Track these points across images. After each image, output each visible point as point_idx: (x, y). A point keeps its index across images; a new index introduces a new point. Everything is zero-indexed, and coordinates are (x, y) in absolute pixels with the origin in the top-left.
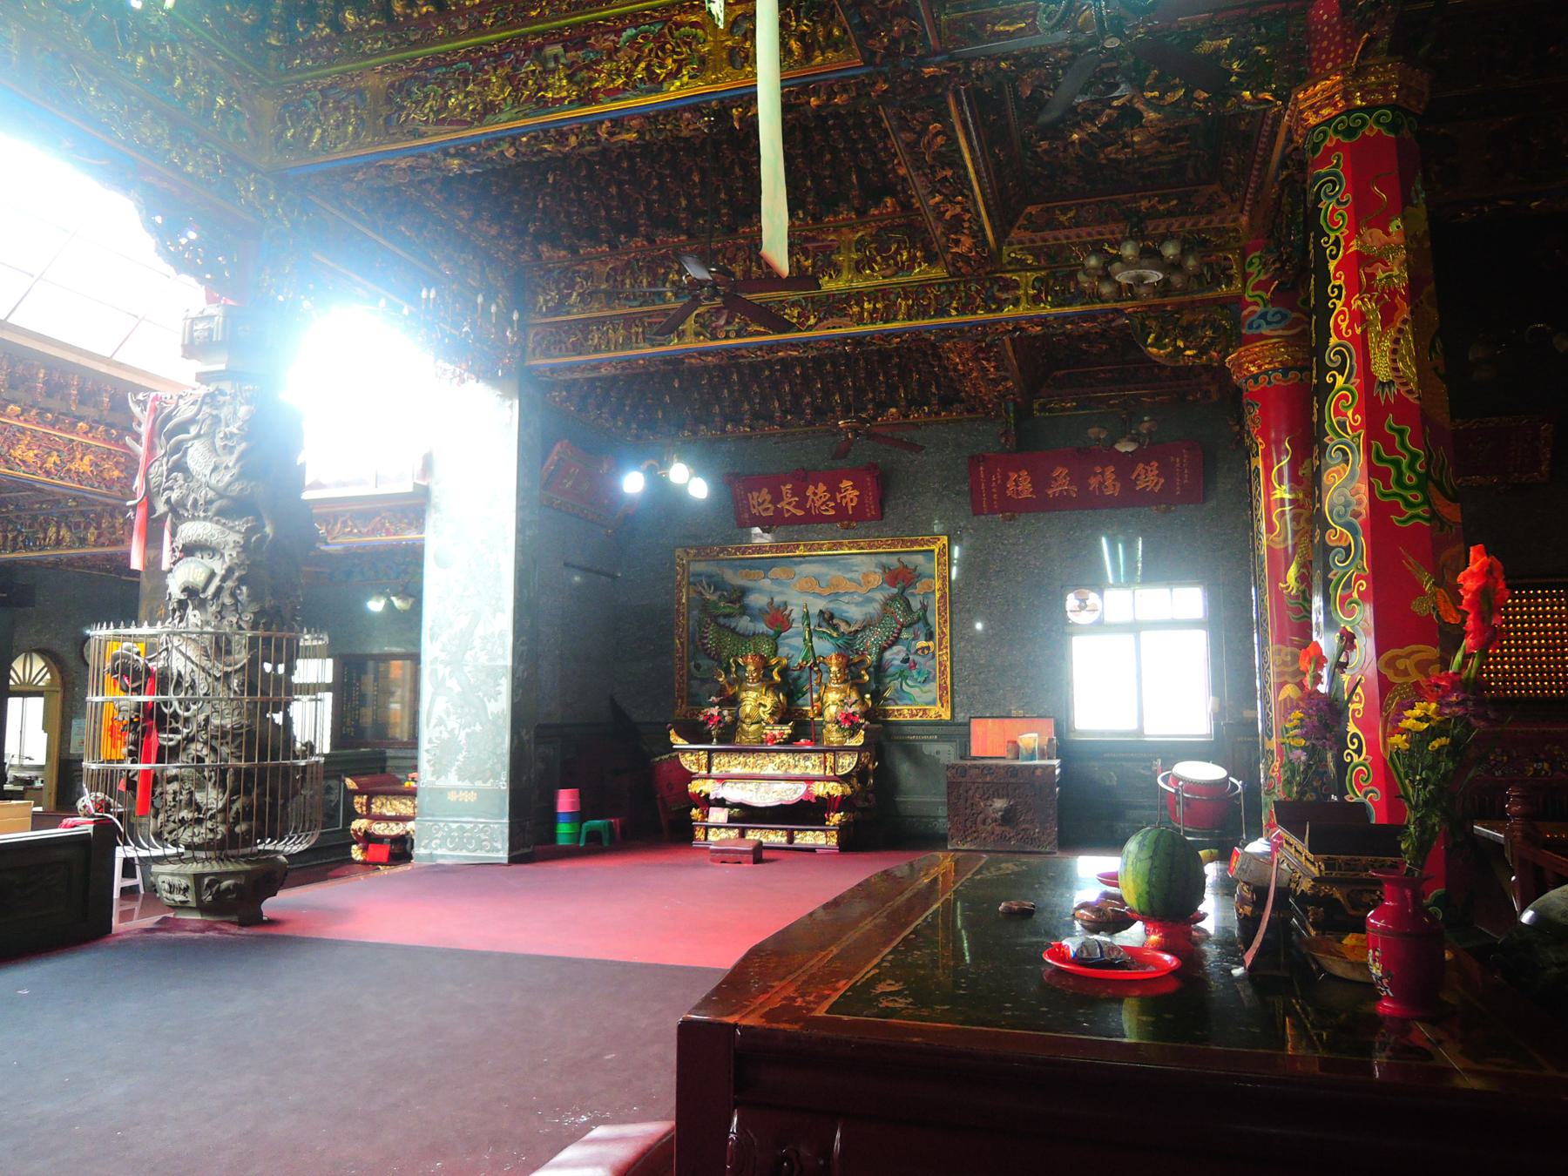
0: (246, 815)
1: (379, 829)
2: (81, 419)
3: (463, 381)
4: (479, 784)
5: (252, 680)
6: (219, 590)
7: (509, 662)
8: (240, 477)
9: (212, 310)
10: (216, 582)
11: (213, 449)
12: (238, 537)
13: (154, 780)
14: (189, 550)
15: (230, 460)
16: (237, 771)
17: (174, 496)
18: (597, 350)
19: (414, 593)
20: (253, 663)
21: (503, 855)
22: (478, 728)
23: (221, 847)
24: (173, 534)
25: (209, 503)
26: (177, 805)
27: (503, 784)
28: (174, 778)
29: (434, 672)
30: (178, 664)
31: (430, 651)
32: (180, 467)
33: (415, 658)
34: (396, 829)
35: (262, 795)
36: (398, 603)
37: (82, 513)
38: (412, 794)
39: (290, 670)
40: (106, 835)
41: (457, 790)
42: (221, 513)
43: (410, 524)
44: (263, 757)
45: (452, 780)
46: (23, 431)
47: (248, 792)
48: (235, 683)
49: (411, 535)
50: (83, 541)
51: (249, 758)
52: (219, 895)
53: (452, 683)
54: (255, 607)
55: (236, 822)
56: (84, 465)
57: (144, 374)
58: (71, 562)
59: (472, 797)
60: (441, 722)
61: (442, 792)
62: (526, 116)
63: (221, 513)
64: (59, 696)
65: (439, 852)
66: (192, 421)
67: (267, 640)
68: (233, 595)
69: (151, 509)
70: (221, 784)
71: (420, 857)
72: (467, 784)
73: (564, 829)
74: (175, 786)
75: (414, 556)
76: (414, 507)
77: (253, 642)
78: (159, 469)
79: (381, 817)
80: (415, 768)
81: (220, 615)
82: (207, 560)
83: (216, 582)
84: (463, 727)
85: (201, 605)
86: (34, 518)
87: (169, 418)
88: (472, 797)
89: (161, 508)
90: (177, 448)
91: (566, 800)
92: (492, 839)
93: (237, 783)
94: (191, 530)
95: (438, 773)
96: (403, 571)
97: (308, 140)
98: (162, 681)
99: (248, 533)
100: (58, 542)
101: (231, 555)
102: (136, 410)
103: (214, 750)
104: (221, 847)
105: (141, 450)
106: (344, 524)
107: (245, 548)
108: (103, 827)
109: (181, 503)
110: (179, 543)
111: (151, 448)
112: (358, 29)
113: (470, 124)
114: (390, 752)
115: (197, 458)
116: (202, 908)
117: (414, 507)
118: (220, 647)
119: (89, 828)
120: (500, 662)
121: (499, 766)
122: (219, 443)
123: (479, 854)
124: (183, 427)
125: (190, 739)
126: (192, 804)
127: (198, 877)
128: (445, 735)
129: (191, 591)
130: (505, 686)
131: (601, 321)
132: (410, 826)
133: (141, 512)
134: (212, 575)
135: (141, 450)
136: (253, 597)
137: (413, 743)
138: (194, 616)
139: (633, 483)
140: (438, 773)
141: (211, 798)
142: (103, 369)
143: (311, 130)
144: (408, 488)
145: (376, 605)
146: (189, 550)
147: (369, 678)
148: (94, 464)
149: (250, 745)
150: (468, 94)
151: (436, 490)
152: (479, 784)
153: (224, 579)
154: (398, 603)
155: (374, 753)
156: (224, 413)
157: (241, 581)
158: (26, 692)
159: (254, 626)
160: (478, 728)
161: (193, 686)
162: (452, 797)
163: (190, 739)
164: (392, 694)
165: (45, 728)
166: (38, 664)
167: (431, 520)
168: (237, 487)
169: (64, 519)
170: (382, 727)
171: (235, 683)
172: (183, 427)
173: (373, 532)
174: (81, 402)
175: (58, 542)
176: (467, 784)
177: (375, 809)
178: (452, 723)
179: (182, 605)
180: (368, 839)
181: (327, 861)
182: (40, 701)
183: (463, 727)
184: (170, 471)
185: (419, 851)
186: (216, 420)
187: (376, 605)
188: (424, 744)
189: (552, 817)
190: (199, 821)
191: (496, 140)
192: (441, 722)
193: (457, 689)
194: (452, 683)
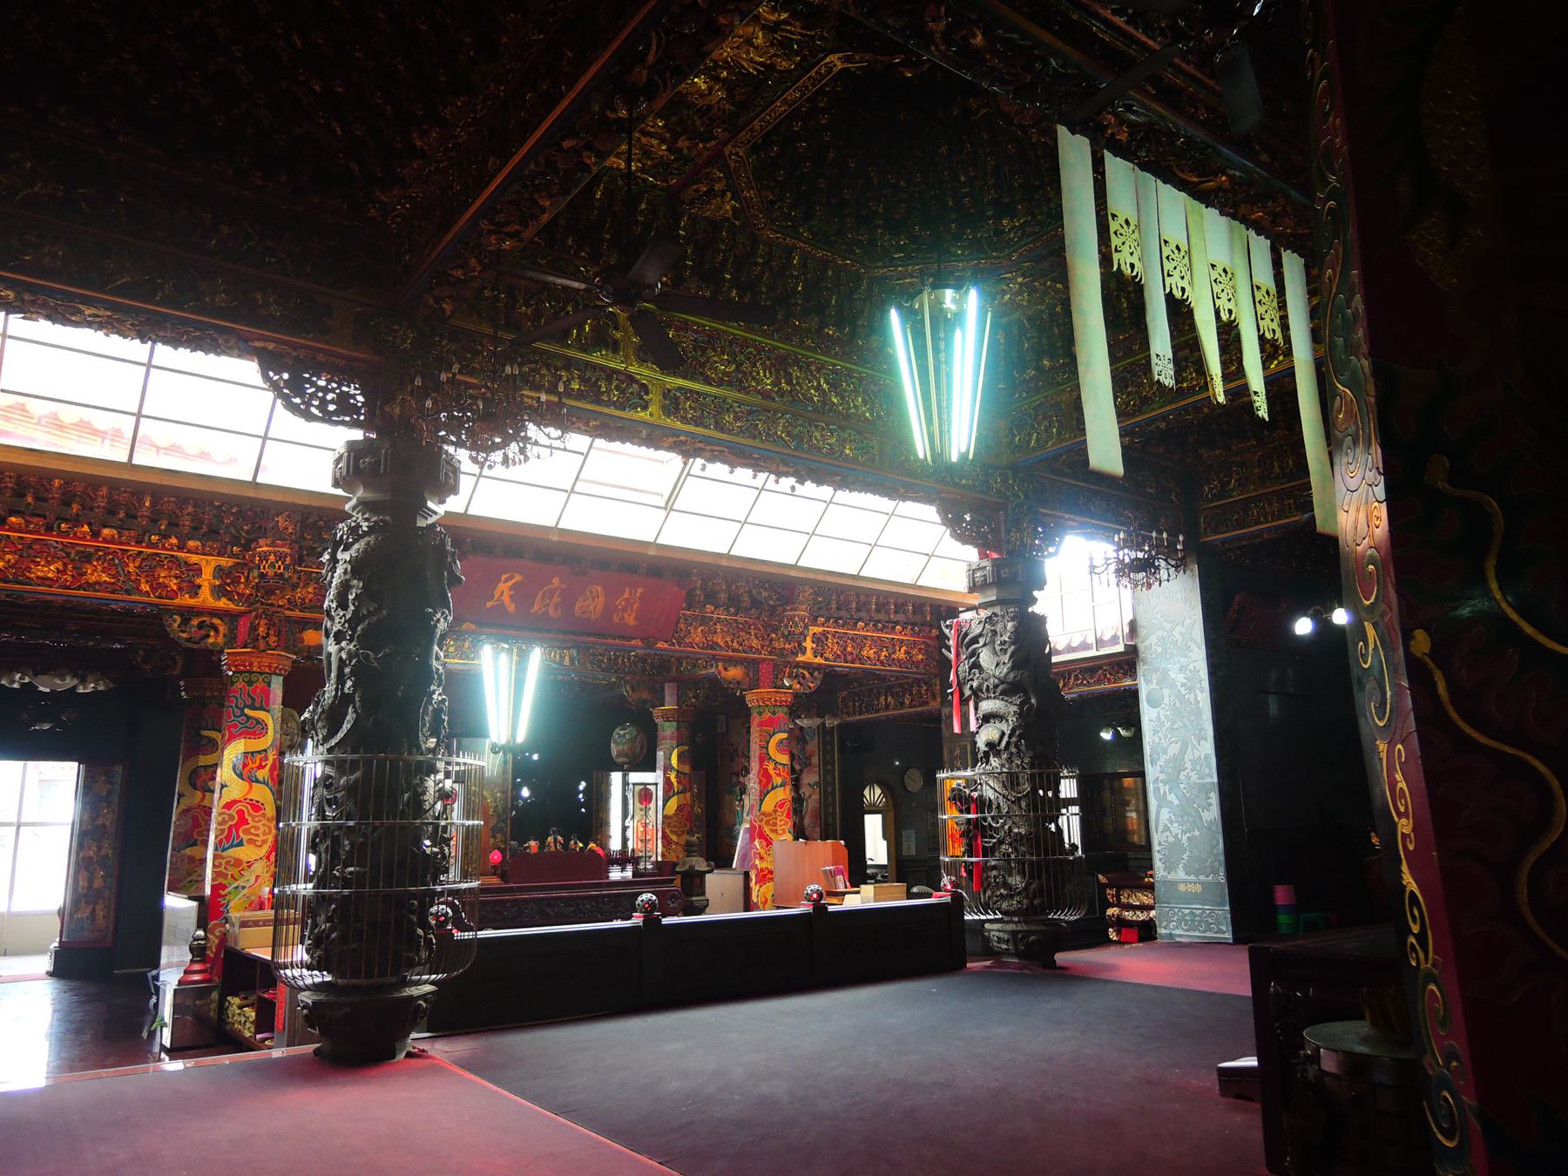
0: (1040, 892)
1: (1128, 915)
2: (897, 623)
3: (1149, 586)
4: (1202, 878)
5: (1034, 801)
6: (1008, 743)
7: (1215, 780)
8: (1012, 669)
9: (985, 563)
10: (1006, 739)
11: (995, 653)
12: (1015, 708)
13: (984, 868)
14: (987, 719)
15: (1006, 658)
16: (1032, 862)
17: (975, 684)
18: (1257, 523)
19: (1134, 722)
20: (1034, 791)
21: (1228, 936)
22: (1197, 833)
23: (1024, 914)
24: (976, 709)
25: (996, 686)
26: (998, 886)
27: (1222, 877)
28: (994, 868)
29: (1157, 790)
30: (989, 794)
31: (1151, 771)
32: (976, 665)
33: (1141, 774)
34: (1142, 916)
35: (1048, 880)
36: (1123, 733)
37: (900, 686)
38: (1150, 888)
39: (1057, 792)
40: (957, 904)
41: (1186, 882)
42: (1003, 693)
43: (1125, 674)
44: (1046, 854)
45: (1180, 874)
46: (866, 637)
47: (1040, 877)
48: (1023, 804)
49: (1128, 682)
50: (902, 704)
51: (1038, 855)
52: (1028, 945)
53: (1172, 797)
54: (1030, 754)
55: (1034, 897)
56: (901, 654)
57: (934, 590)
58: (895, 718)
59: (1199, 888)
60: (1166, 829)
61: (1174, 884)
62: (1170, 403)
63: (1003, 693)
64: (892, 814)
65: (1177, 932)
66: (980, 635)
67: (1041, 775)
68: (1017, 746)
69: (962, 694)
70: (1022, 873)
71: (1162, 936)
72: (1192, 877)
73: (1283, 919)
74: (994, 873)
75: (1133, 694)
76: (1128, 662)
77: (1032, 776)
78: (964, 667)
79: (1130, 906)
80: (1151, 867)
81: (1010, 760)
82: (998, 724)
83: (1006, 739)
84: (1184, 832)
85: (998, 754)
86: (871, 690)
87: (966, 635)
88: (1199, 888)
89: (967, 692)
90: (974, 654)
91: (1282, 895)
92: (1218, 923)
93: (1032, 871)
94: (987, 706)
95: (1169, 869)
96: (1126, 708)
97: (1029, 441)
98: (982, 804)
99: (1021, 706)
100: (887, 707)
101: (1012, 719)
102: (947, 631)
103: (1016, 849)
104: (1024, 914)
105: (952, 656)
106: (1077, 678)
107: (1020, 715)
108: (957, 898)
109: (980, 688)
110: (980, 714)
111: (958, 655)
112: (1052, 368)
113: (1134, 416)
114: (1131, 855)
115: (985, 658)
116: (1018, 954)
117: (1128, 662)
118: (1011, 781)
119: (948, 899)
120: (1208, 780)
121: (1216, 865)
122: (998, 648)
123: (1208, 934)
124: (975, 640)
125: (1001, 842)
126: (1006, 885)
127: (1014, 933)
128: (1171, 839)
129: (990, 744)
130: (1214, 798)
131: (1259, 498)
132: (1153, 913)
133: (956, 697)
134: (1003, 734)
135: (952, 656)
136: (1028, 747)
137: (1148, 847)
138: (994, 762)
139: (1303, 626)
140: (1169, 869)
141: (1016, 881)
142: (911, 592)
143: (1030, 435)
144: (1120, 648)
145: (1106, 735)
146: (987, 719)
147: (1107, 794)
148: (907, 652)
149: (1038, 844)
150: (1129, 394)
151: (1141, 647)
152: (1202, 878)
153: (1010, 736)
154: (1123, 733)
155: (1121, 854)
156: (999, 628)
157: (1020, 737)
158: (874, 811)
159: (1032, 766)
160: (1197, 833)
161: (998, 807)
162: (1182, 888)
163: (1001, 842)
164: (1127, 803)
165: (885, 837)
166: (878, 791)
167: (1141, 669)
168: (1012, 675)
169: (889, 690)
170: (1122, 832)
171: (1023, 804)
172: (975, 640)
173: (1098, 682)
174: (896, 612)
175: (887, 707)
176: (1192, 877)
177: (1124, 900)
178: (1175, 828)
179: (986, 755)
180: (1121, 923)
181: (1093, 934)
182: (879, 817)
183: (1184, 832)
184: (971, 668)
185: (1161, 931)
186: (994, 633)
187: (1106, 735)
188: (1156, 847)
189: (1272, 910)
190: (1012, 897)
191: (1151, 421)
192: (1166, 829)
193: (1176, 802)
194: (1172, 797)
